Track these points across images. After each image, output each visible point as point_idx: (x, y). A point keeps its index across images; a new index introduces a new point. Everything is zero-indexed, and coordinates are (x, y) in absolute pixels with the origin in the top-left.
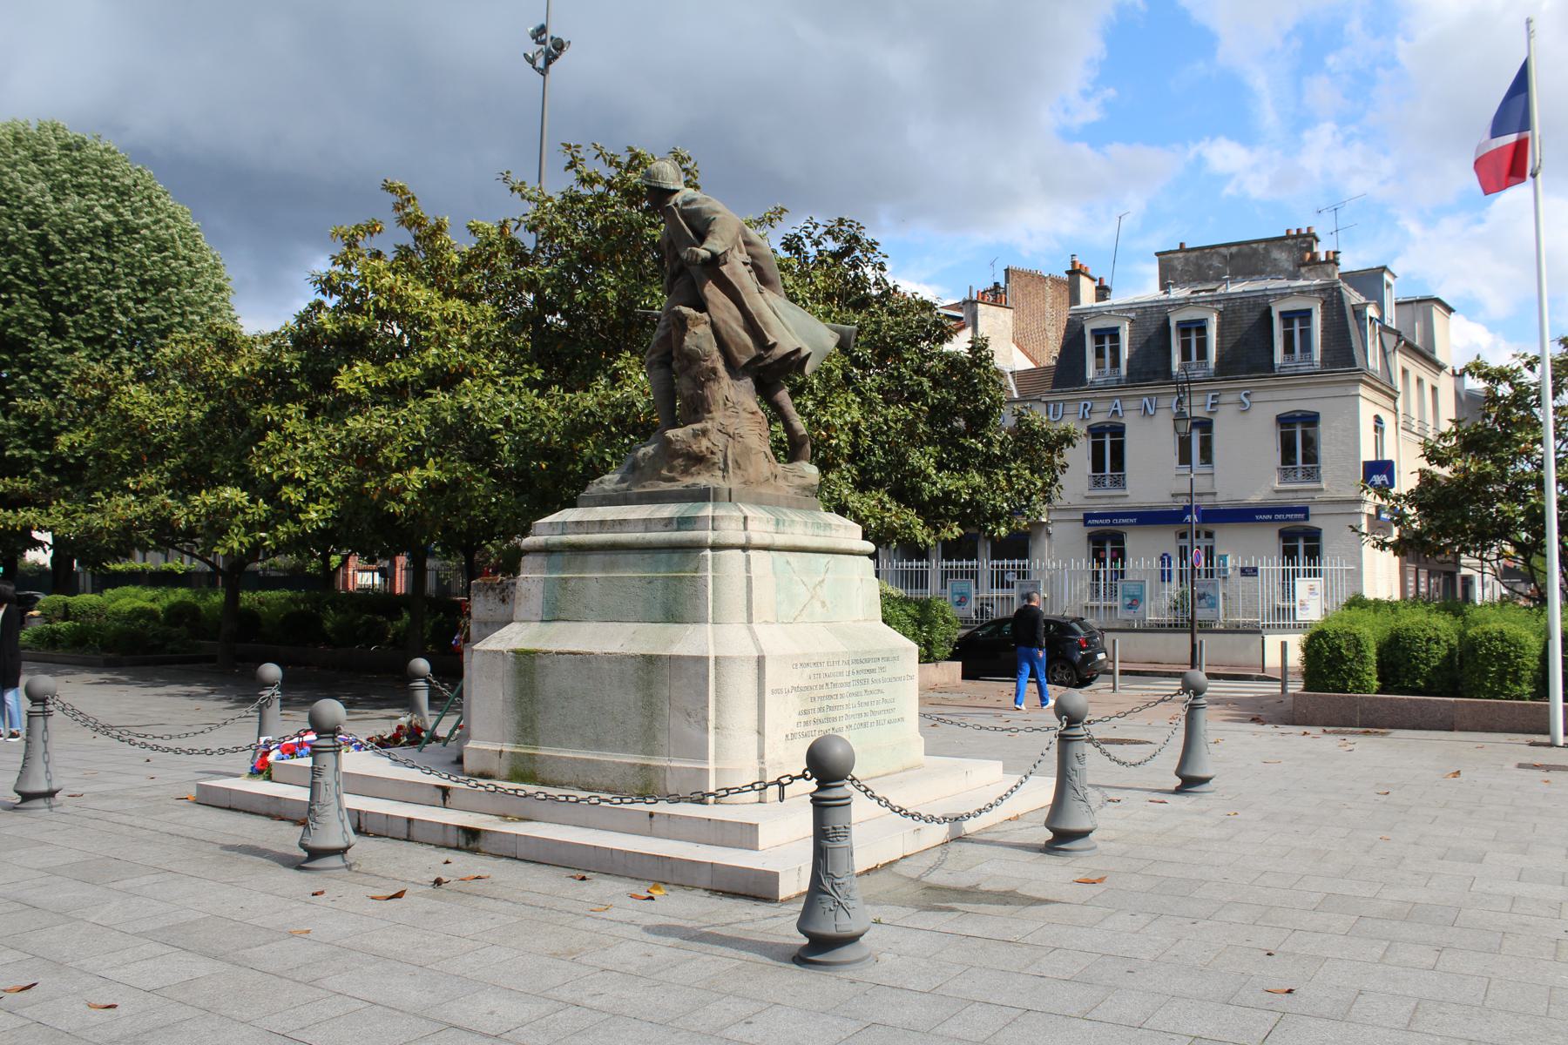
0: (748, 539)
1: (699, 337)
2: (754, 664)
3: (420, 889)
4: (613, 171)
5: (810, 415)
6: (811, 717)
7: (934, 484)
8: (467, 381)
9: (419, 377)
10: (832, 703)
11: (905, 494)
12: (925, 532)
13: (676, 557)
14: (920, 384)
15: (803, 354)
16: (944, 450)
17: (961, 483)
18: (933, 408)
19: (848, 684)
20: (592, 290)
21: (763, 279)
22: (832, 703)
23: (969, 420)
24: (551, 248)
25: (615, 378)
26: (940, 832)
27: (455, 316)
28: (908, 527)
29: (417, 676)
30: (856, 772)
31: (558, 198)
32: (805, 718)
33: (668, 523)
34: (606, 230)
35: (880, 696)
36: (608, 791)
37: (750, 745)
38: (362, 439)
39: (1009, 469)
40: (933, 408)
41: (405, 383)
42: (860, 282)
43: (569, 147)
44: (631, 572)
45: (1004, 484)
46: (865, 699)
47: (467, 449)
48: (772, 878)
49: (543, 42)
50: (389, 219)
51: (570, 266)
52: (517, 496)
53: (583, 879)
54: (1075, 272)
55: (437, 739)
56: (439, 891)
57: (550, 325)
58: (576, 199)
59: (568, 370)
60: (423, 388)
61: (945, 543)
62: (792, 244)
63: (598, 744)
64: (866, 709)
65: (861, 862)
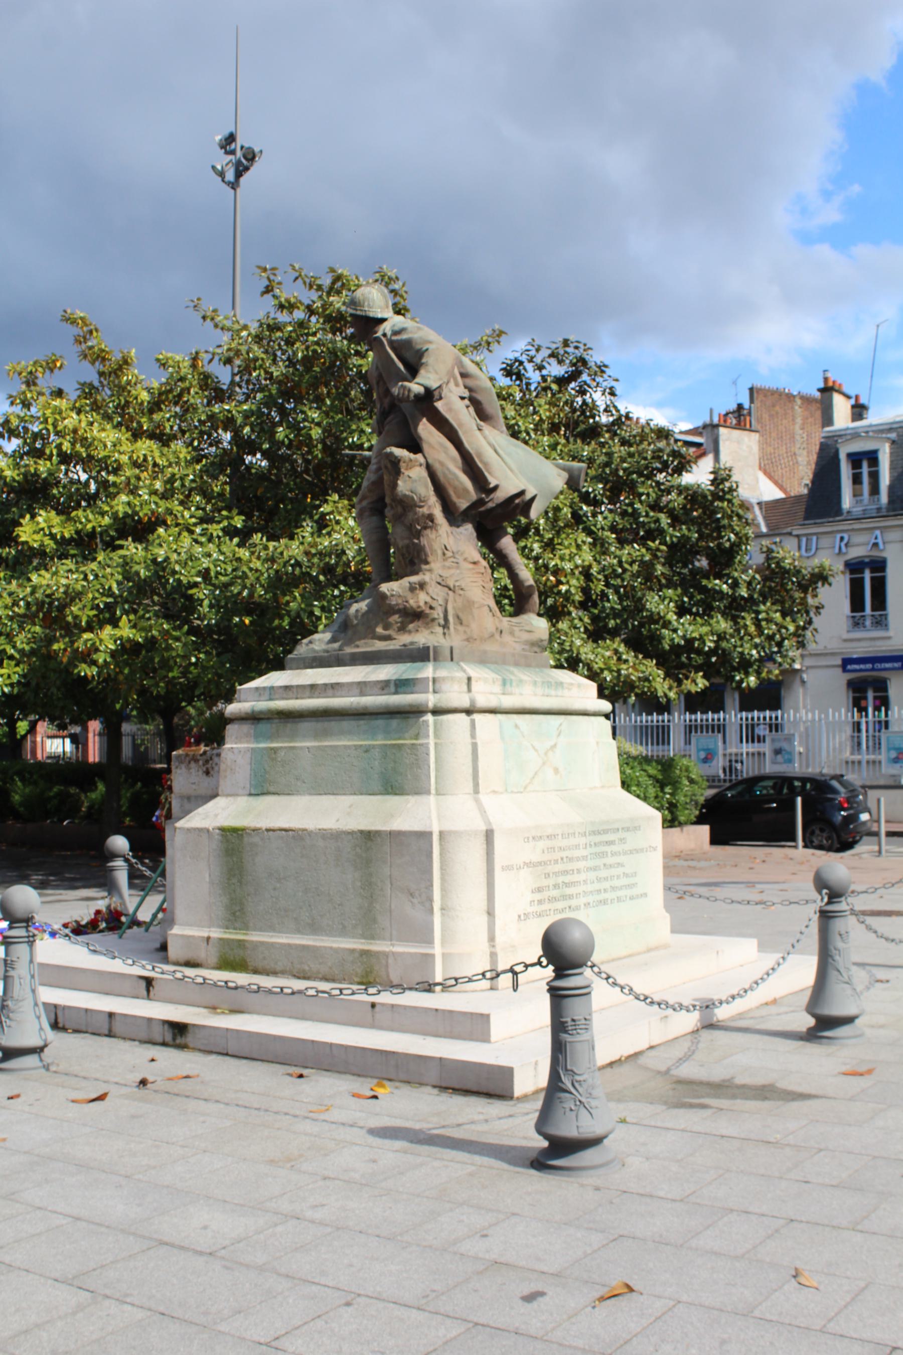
0: (473, 702)
1: (413, 481)
2: (482, 840)
3: (124, 1090)
4: (314, 295)
5: (536, 559)
6: (546, 894)
7: (675, 631)
8: (161, 530)
9: (109, 527)
10: (567, 879)
11: (643, 642)
12: (666, 686)
13: (394, 723)
14: (657, 521)
15: (528, 496)
16: (685, 593)
17: (705, 629)
18: (672, 547)
19: (585, 858)
20: (295, 427)
21: (482, 414)
22: (567, 879)
23: (711, 555)
24: (248, 382)
25: (322, 524)
26: (692, 1020)
27: (145, 460)
28: (646, 679)
29: (113, 856)
30: (595, 958)
31: (254, 328)
32: (538, 896)
33: (385, 686)
34: (308, 362)
35: (620, 871)
36: (326, 979)
37: (480, 929)
38: (48, 596)
39: (758, 613)
40: (672, 547)
41: (92, 534)
42: (588, 409)
43: (265, 270)
44: (346, 740)
45: (752, 629)
46: (603, 873)
47: (163, 605)
48: (506, 1074)
49: (233, 152)
50: (70, 355)
51: (269, 402)
52: (218, 655)
53: (301, 1076)
54: (828, 390)
55: (139, 924)
56: (143, 1092)
57: (249, 468)
58: (274, 327)
59: (271, 514)
60: (113, 539)
61: (689, 696)
62: (512, 371)
63: (314, 928)
64: (606, 885)
65: (603, 1056)
